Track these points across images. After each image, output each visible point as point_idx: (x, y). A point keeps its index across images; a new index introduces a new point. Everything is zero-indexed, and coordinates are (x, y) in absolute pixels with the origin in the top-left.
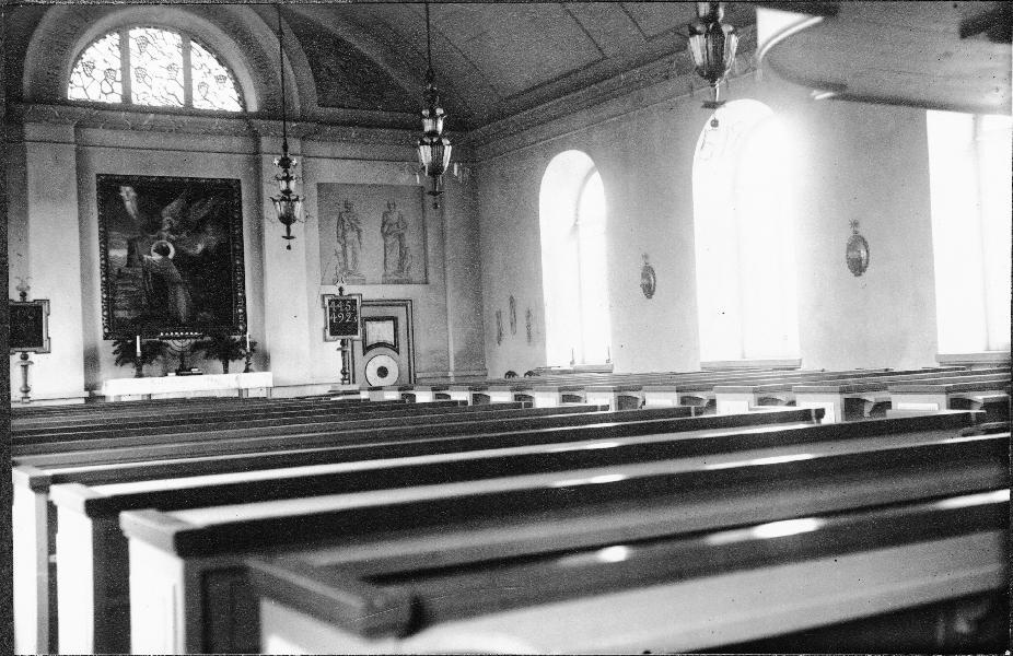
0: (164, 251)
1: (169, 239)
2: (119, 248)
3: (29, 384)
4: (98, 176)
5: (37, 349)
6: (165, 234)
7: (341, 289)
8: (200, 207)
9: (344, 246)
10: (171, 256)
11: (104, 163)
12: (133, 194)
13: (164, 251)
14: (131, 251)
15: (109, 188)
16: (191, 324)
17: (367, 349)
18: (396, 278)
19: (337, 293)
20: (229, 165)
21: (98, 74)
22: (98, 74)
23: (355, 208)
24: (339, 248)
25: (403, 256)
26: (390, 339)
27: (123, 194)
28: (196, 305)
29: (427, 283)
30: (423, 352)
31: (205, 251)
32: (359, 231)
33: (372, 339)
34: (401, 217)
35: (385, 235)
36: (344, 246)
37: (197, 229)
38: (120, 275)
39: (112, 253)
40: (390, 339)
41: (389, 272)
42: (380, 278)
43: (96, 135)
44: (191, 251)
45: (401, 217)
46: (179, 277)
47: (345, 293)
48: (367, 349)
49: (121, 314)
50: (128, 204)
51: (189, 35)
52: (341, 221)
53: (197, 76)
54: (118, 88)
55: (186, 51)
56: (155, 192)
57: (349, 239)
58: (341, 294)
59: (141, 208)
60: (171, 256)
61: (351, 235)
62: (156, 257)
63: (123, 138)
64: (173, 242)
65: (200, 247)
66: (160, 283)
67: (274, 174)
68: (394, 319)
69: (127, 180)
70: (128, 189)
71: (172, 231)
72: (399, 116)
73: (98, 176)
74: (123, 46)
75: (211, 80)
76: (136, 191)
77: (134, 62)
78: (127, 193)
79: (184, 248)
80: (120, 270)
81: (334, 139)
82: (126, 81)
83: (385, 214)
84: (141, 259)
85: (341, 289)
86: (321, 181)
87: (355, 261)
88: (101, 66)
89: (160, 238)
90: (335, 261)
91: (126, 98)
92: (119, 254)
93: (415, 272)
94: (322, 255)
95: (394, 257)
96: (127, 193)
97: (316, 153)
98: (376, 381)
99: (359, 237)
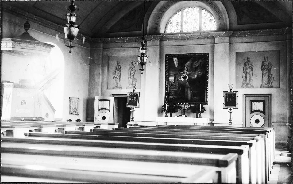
0: (185, 78)
1: (186, 74)
2: (172, 76)
3: (231, 118)
4: (166, 55)
5: (234, 107)
6: (185, 72)
7: (134, 90)
8: (197, 63)
9: (246, 74)
10: (187, 79)
11: (169, 51)
12: (177, 60)
13: (185, 78)
14: (175, 78)
15: (169, 58)
16: (191, 102)
17: (251, 112)
18: (266, 86)
19: (132, 92)
20: (205, 49)
21: (174, 24)
22: (174, 24)
23: (251, 60)
24: (244, 75)
25: (270, 78)
26: (261, 109)
27: (174, 60)
28: (193, 95)
29: (279, 88)
30: (275, 115)
31: (197, 77)
32: (252, 69)
33: (254, 108)
34: (270, 63)
35: (262, 70)
36: (246, 74)
37: (195, 70)
38: (172, 85)
39: (170, 78)
40: (261, 109)
41: (263, 84)
42: (259, 86)
43: (165, 43)
44: (193, 77)
45: (270, 63)
46: (189, 86)
47: (135, 92)
48: (251, 112)
49: (171, 97)
50: (175, 63)
51: (202, 8)
52: (245, 65)
53: (203, 20)
54: (179, 28)
55: (201, 12)
56: (183, 58)
57: (248, 72)
58: (134, 92)
59: (179, 64)
60: (187, 79)
61: (249, 70)
62: (182, 79)
63: (174, 43)
64: (187, 74)
65: (196, 76)
66: (183, 87)
67: (138, 52)
68: (109, 100)
69: (175, 56)
70: (175, 58)
71: (188, 71)
72: (273, 24)
73: (166, 55)
74: (182, 16)
75: (208, 22)
76: (178, 59)
77: (184, 19)
78: (175, 60)
79: (191, 76)
80: (172, 84)
81: (239, 36)
82: (182, 26)
83: (263, 62)
84: (178, 80)
85: (134, 90)
86: (237, 51)
87: (250, 79)
88: (175, 22)
89: (184, 73)
90: (242, 80)
91: (200, 29)
92: (172, 79)
93: (274, 84)
94: (237, 77)
95: (266, 78)
96: (175, 60)
97: (112, 46)
98: (101, 121)
99: (252, 71)
